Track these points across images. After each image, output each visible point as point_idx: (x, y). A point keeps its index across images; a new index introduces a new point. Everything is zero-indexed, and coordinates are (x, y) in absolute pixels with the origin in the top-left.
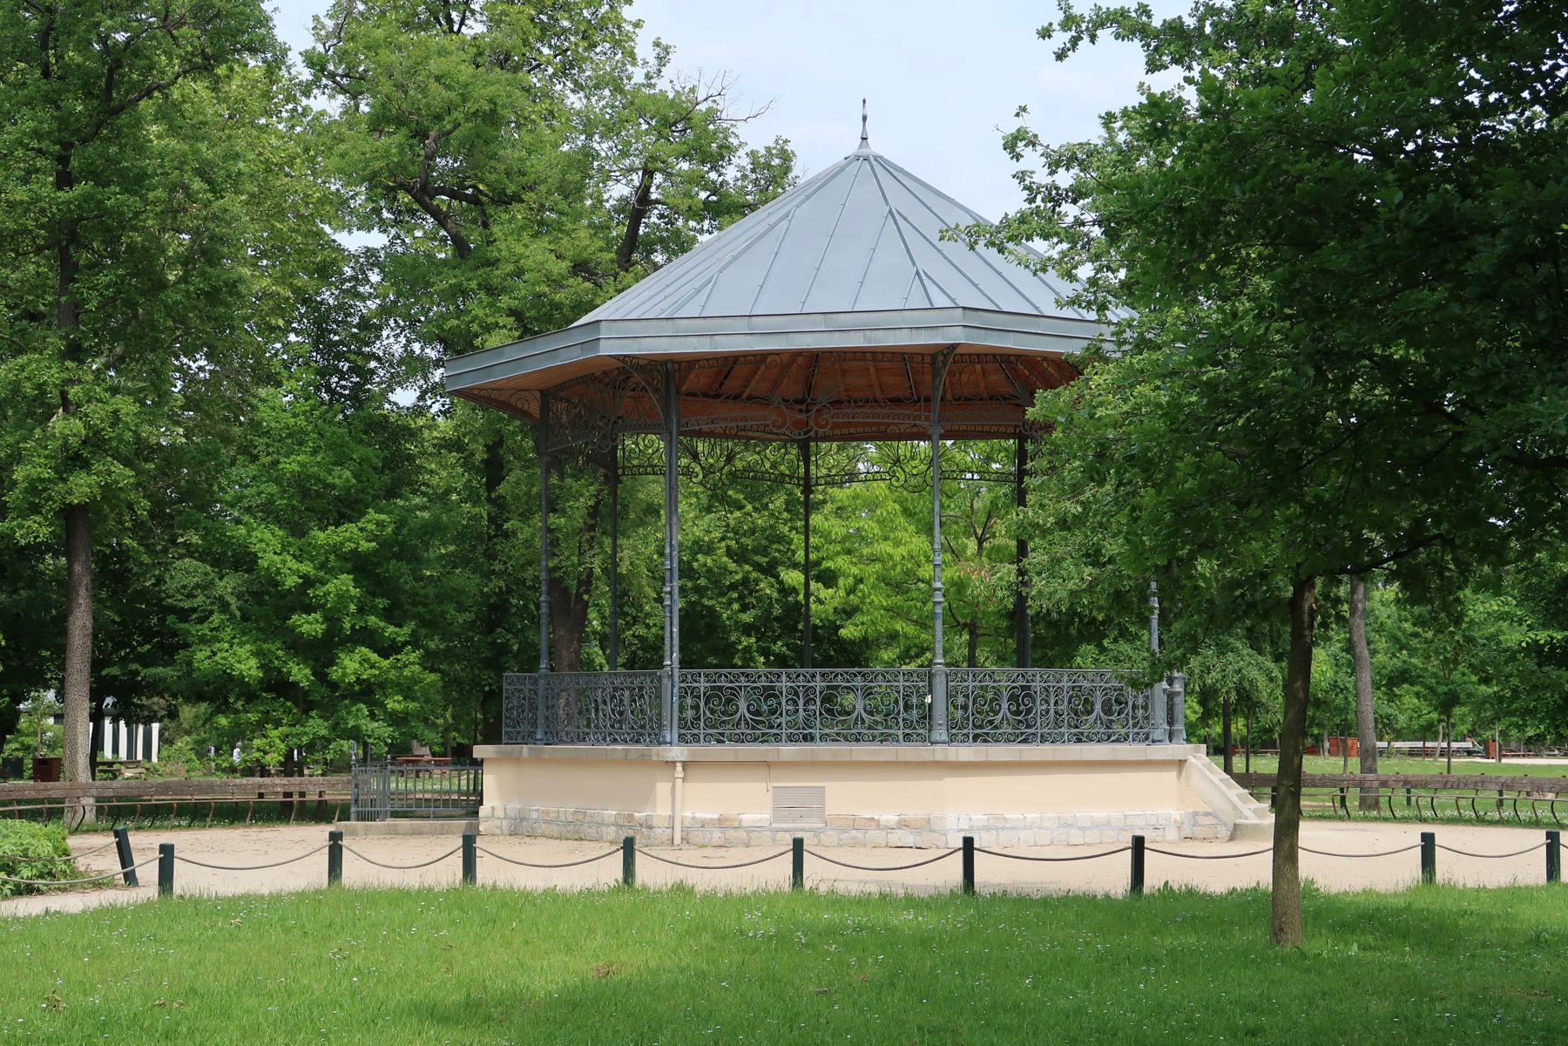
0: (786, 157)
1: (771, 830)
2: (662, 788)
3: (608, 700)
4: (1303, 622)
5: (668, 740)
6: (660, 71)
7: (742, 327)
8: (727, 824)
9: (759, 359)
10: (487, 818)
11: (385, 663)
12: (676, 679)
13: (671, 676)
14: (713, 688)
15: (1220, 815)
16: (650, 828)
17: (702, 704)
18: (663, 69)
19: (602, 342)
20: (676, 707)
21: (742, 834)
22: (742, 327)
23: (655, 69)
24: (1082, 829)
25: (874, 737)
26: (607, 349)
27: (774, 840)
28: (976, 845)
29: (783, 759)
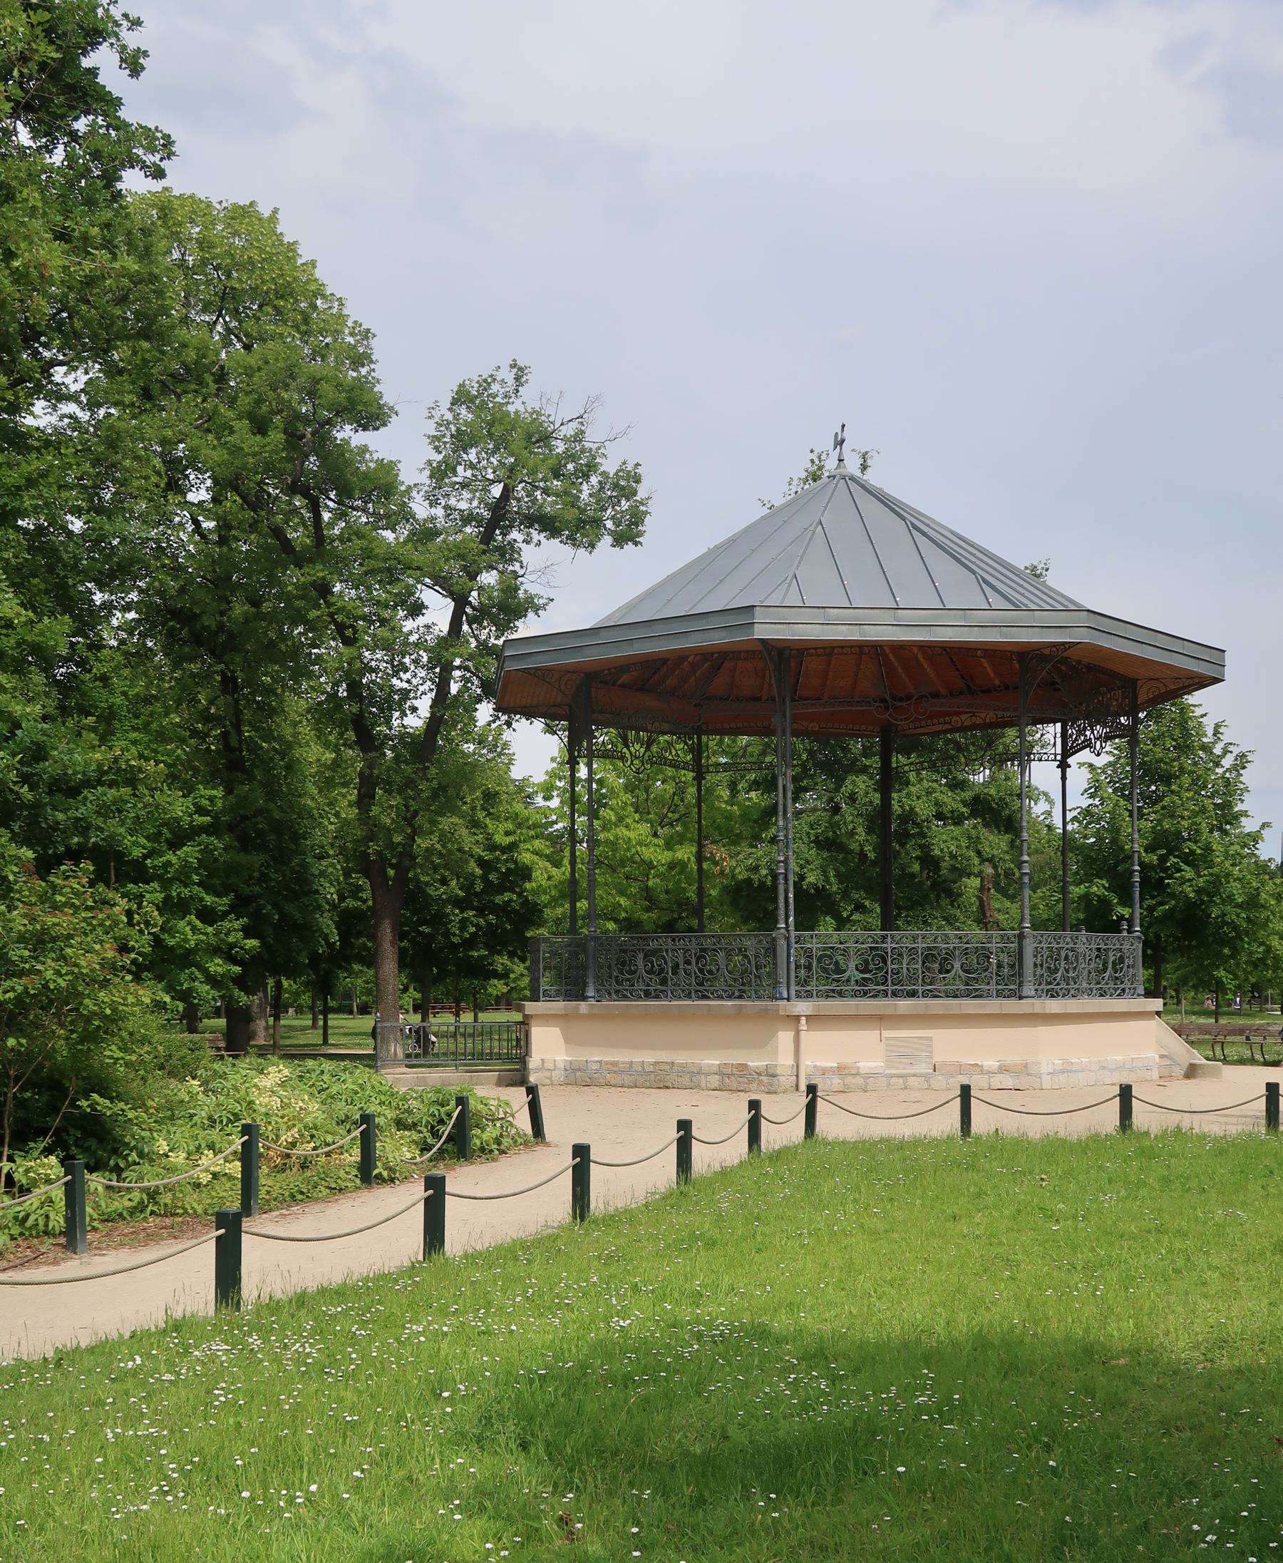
3: (694, 961)
4: (356, 909)
5: (785, 995)
6: (518, 391)
7: (888, 617)
9: (681, 657)
10: (537, 1070)
11: (210, 929)
12: (793, 940)
13: (787, 939)
16: (774, 1076)
17: (814, 964)
18: (520, 388)
19: (756, 625)
20: (793, 966)
21: (859, 1080)
22: (888, 617)
23: (512, 389)
24: (1111, 1070)
25: (865, 994)
27: (889, 1085)
29: (901, 1012)
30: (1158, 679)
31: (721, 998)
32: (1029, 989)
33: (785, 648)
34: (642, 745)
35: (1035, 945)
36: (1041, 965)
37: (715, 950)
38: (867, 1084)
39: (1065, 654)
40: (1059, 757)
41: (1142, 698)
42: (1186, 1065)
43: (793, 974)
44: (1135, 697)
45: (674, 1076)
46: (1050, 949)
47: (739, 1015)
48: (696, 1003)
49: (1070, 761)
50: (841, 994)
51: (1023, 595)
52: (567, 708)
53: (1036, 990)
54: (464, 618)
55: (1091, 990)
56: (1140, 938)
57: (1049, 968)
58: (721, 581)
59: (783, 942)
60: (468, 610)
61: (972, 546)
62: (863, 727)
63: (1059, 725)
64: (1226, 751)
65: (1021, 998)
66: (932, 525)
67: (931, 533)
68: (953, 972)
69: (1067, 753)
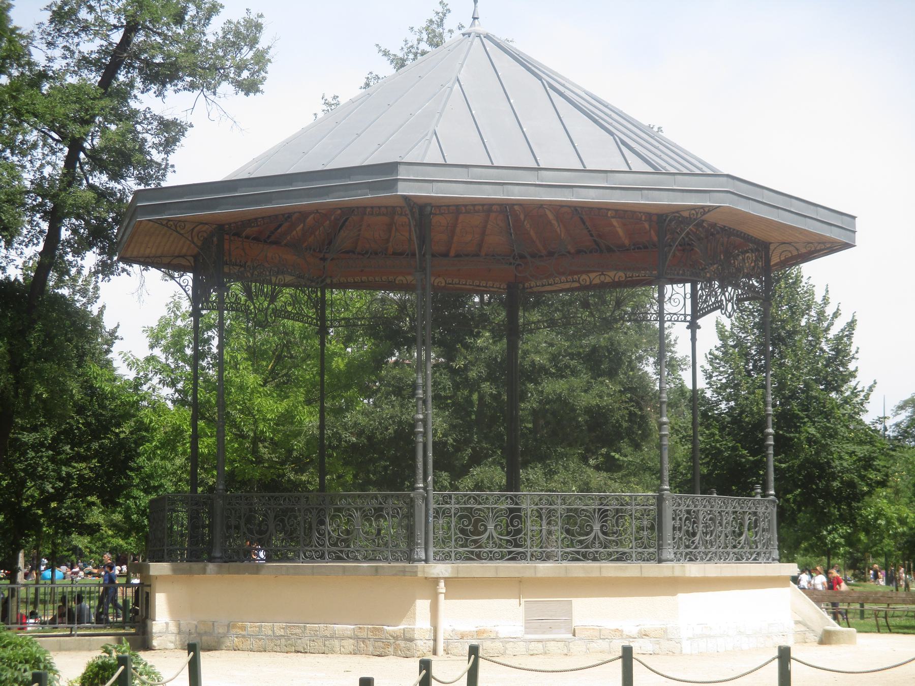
0: (258, 27)
1: (525, 641)
2: (422, 606)
7: (531, 178)
8: (485, 635)
10: (161, 634)
13: (426, 500)
14: (569, 510)
15: (809, 623)
16: (411, 640)
22: (531, 178)
26: (404, 190)
28: (792, 655)
30: (789, 243)
31: (356, 559)
32: (668, 553)
33: (426, 205)
34: (266, 297)
35: (674, 508)
36: (680, 529)
37: (349, 510)
38: (506, 649)
39: (704, 217)
40: (689, 318)
41: (775, 260)
42: (820, 631)
43: (431, 535)
44: (768, 260)
45: (305, 640)
46: (688, 512)
47: (297, 572)
48: (392, 564)
49: (700, 322)
50: (479, 557)
51: (659, 157)
52: (192, 259)
53: (675, 553)
54: (78, 165)
55: (728, 554)
56: (774, 502)
57: (687, 531)
58: (358, 135)
59: (420, 503)
60: (82, 155)
61: (606, 107)
62: (490, 283)
63: (688, 286)
64: (836, 315)
65: (660, 561)
66: (567, 85)
67: (568, 93)
68: (592, 535)
69: (697, 314)
